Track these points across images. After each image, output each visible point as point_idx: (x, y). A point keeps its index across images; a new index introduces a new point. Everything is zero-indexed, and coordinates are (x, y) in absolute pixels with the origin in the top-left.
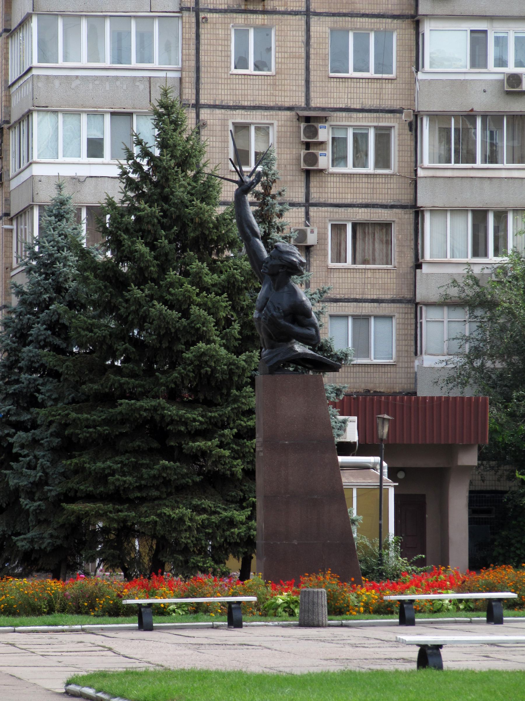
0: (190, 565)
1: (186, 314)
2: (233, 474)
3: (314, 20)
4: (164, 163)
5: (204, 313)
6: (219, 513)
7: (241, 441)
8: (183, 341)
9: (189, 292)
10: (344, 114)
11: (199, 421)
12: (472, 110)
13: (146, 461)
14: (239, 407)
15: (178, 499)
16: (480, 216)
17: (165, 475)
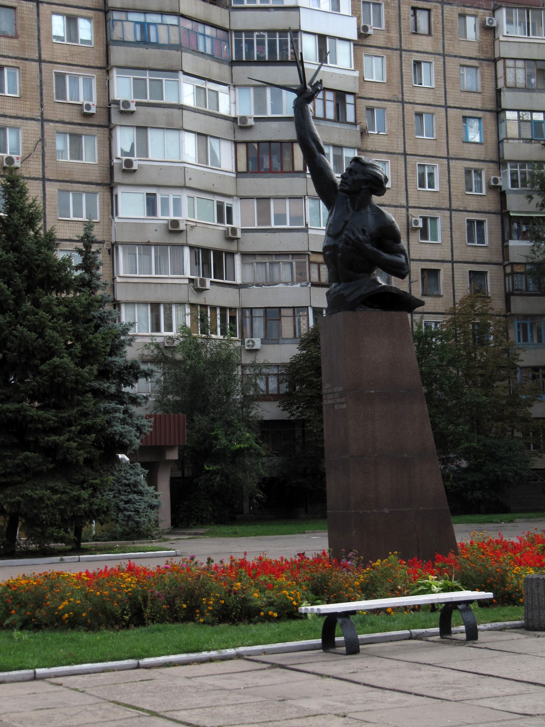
0: (46, 535)
1: (41, 335)
2: (77, 462)
3: (47, 184)
4: (16, 221)
5: (56, 335)
6: (67, 493)
7: (83, 436)
8: (38, 357)
9: (43, 318)
10: (68, 243)
11: (52, 420)
12: (149, 242)
13: (9, 453)
14: (82, 409)
15: (36, 483)
16: (155, 306)
17: (26, 464)
